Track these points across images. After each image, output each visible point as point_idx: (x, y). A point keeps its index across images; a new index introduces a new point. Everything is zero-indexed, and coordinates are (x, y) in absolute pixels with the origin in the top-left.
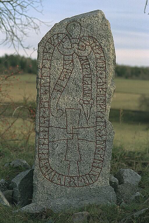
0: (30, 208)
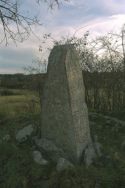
0: (88, 161)
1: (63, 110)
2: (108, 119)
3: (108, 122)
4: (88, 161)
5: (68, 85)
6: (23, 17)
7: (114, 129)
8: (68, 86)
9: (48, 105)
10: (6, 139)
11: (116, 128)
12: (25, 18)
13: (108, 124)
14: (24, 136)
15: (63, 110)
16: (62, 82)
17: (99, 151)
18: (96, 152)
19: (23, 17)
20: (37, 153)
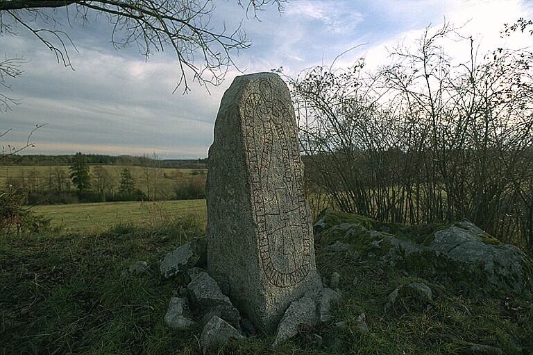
0: (286, 330)
1: (239, 210)
2: (377, 238)
3: (376, 243)
4: (286, 330)
5: (245, 154)
6: (213, 35)
7: (385, 261)
8: (244, 156)
9: (216, 200)
10: (135, 270)
11: (390, 257)
12: (217, 37)
13: (373, 249)
14: (175, 265)
15: (239, 210)
16: (234, 148)
17: (324, 309)
18: (317, 312)
19: (213, 35)
20: (176, 302)
